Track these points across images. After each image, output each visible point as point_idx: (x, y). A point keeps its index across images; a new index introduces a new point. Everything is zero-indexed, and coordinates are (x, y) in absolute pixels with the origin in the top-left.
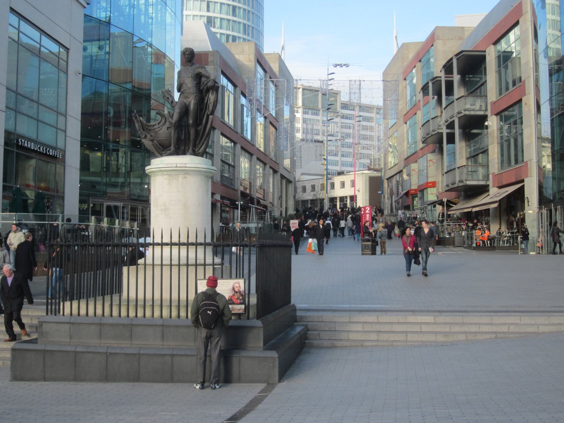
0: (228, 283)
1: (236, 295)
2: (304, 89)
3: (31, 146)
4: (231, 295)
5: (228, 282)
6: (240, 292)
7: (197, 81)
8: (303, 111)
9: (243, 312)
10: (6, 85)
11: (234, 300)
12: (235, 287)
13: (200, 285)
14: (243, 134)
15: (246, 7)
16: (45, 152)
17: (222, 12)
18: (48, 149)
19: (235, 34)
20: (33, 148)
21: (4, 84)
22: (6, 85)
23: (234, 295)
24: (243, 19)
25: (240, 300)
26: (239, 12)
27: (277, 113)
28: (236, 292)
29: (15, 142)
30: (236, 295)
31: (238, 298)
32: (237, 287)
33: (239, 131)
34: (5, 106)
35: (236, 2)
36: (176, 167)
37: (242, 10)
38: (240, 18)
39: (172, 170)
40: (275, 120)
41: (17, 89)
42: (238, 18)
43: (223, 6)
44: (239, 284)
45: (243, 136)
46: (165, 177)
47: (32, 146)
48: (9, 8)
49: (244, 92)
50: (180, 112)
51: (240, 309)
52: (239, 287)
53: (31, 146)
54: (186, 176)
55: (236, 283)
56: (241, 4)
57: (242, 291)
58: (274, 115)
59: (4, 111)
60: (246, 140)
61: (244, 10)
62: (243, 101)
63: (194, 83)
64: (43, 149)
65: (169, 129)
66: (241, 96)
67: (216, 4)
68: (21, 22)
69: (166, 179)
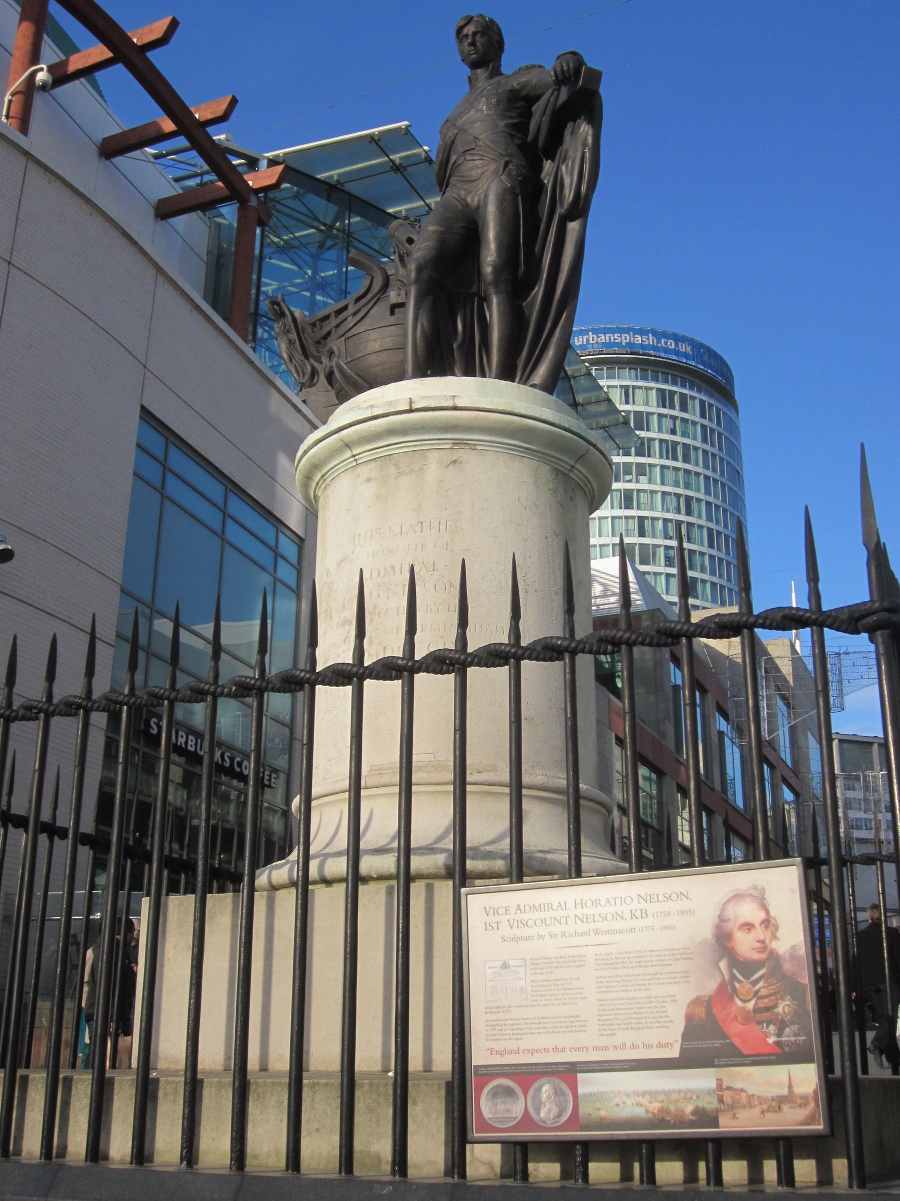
0: (685, 904)
1: (744, 986)
2: (841, 741)
3: (186, 743)
4: (710, 986)
5: (682, 895)
6: (773, 956)
7: (511, 118)
8: (845, 785)
9: (811, 1120)
10: (120, 582)
11: (735, 1029)
12: (732, 926)
13: (488, 926)
14: (727, 795)
15: (715, 579)
16: (227, 765)
17: (670, 591)
18: (238, 759)
19: (691, 493)
20: (192, 749)
21: (115, 579)
22: (120, 582)
23: (725, 992)
24: (710, 574)
25: (781, 1026)
26: (704, 589)
27: (794, 761)
28: (747, 967)
29: (142, 727)
30: (744, 986)
31: (763, 1016)
32: (748, 926)
33: (717, 785)
34: (115, 634)
35: (697, 571)
36: (411, 411)
37: (708, 585)
38: (707, 600)
39: (392, 432)
40: (793, 775)
41: (153, 599)
42: (702, 600)
43: (667, 497)
44: (764, 907)
45: (726, 798)
46: (364, 471)
47: (190, 743)
48: (139, 408)
49: (721, 703)
50: (442, 233)
51: (780, 1102)
52: (767, 922)
53: (186, 743)
54: (461, 454)
55: (738, 897)
56: (706, 573)
57: (793, 957)
58: (789, 763)
59: (113, 643)
60: (735, 809)
61: (713, 584)
62: (722, 725)
63: (502, 124)
64: (222, 755)
65: (397, 310)
66: (717, 714)
67: (658, 577)
68: (171, 447)
69: (368, 480)
